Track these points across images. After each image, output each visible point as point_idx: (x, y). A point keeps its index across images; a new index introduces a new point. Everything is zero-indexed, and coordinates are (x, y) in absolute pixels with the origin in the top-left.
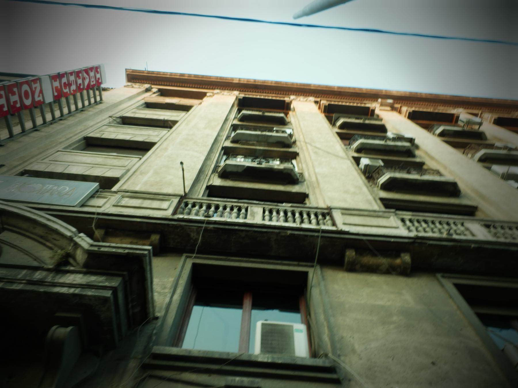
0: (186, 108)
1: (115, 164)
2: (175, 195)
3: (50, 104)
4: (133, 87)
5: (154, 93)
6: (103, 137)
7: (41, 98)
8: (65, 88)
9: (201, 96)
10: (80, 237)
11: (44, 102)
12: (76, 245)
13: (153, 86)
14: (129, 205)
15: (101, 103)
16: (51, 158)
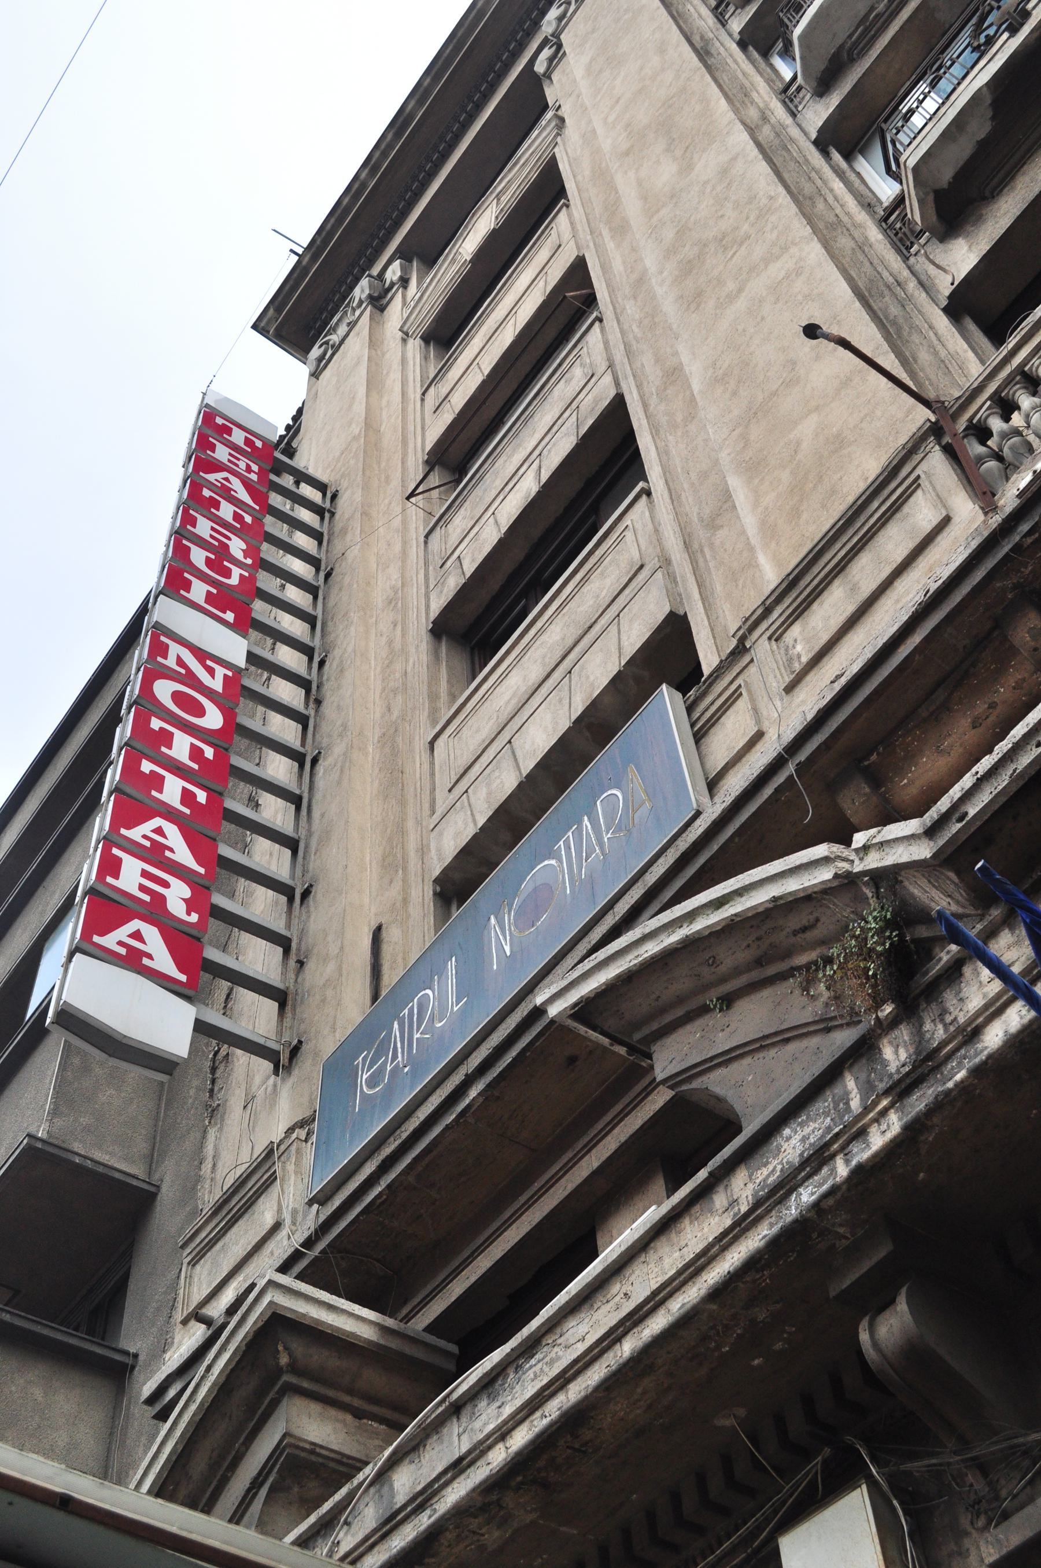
0: (547, 193)
1: (606, 596)
2: (912, 450)
3: (252, 658)
4: (336, 348)
5: (404, 282)
6: (470, 567)
7: (220, 672)
8: (228, 574)
9: (530, 104)
10: (866, 848)
11: (237, 671)
12: (886, 879)
13: (375, 271)
14: (825, 637)
15: (334, 497)
16: (443, 781)
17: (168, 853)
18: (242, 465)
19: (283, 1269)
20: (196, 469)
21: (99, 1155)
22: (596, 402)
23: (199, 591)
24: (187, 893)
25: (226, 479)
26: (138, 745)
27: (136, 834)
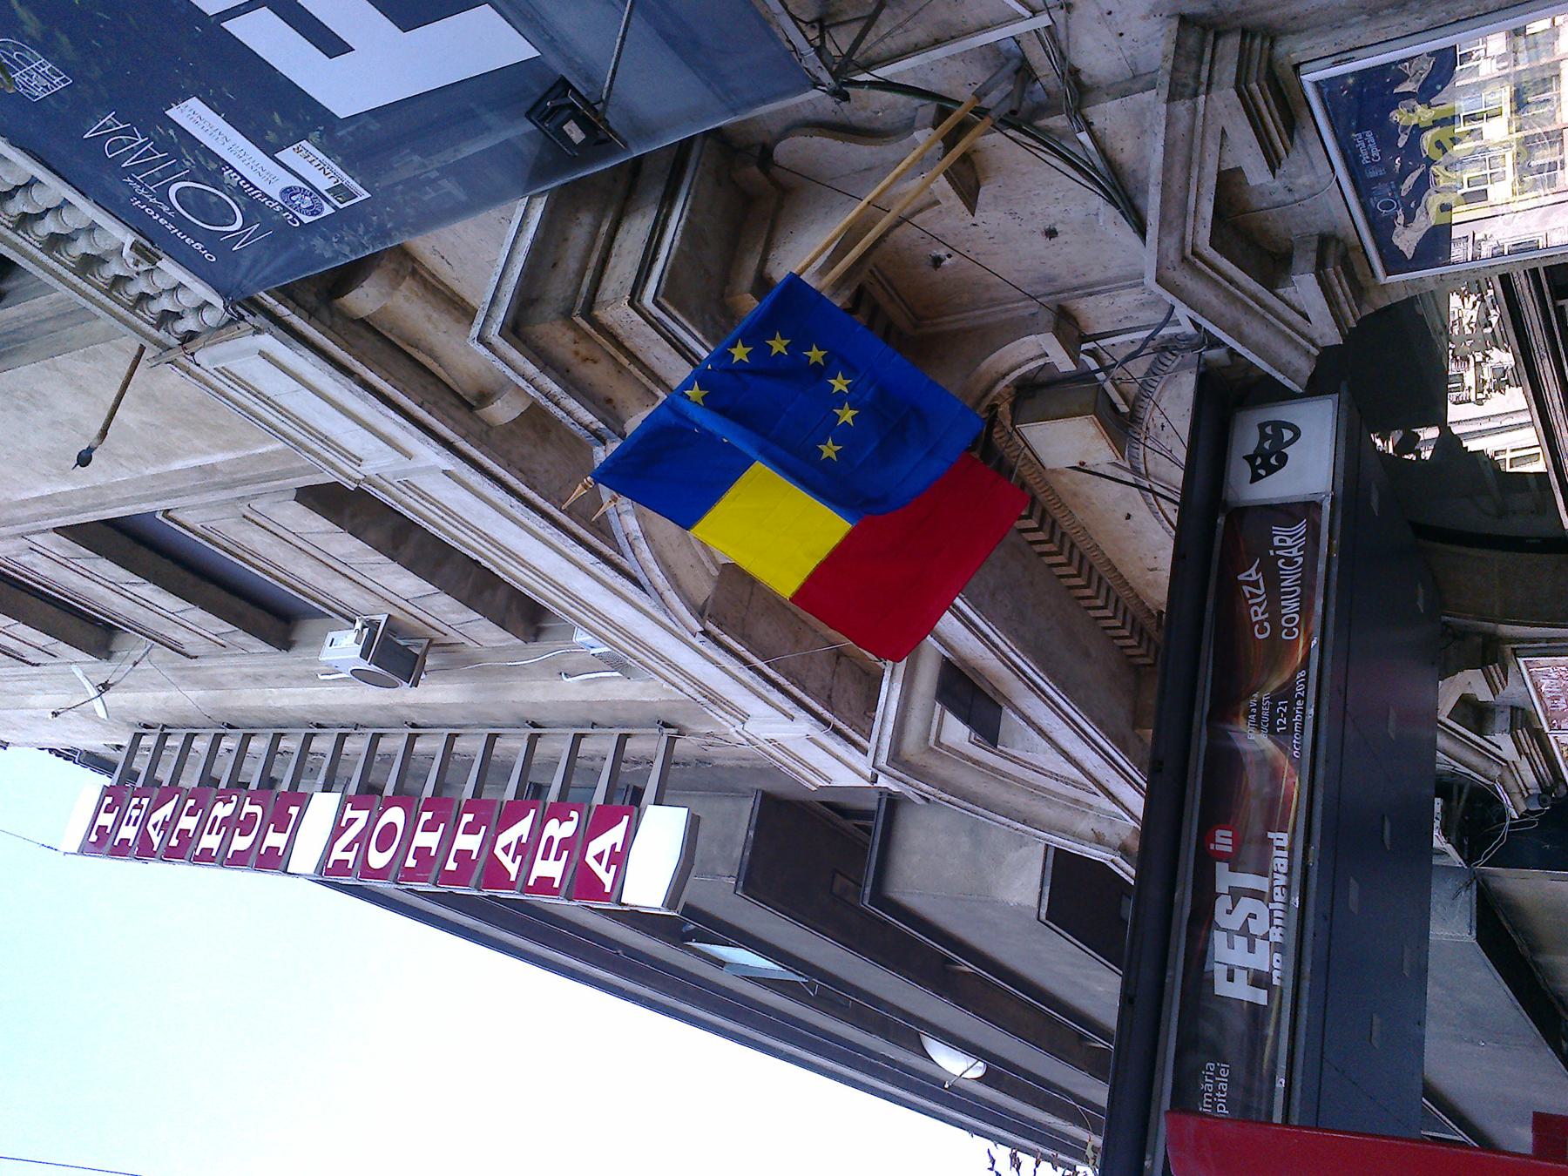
8: (251, 817)
17: (524, 840)
18: (136, 813)
19: (865, 752)
20: (152, 855)
21: (741, 837)
22: (60, 546)
23: (275, 839)
24: (554, 823)
25: (155, 826)
26: (433, 875)
27: (513, 869)
